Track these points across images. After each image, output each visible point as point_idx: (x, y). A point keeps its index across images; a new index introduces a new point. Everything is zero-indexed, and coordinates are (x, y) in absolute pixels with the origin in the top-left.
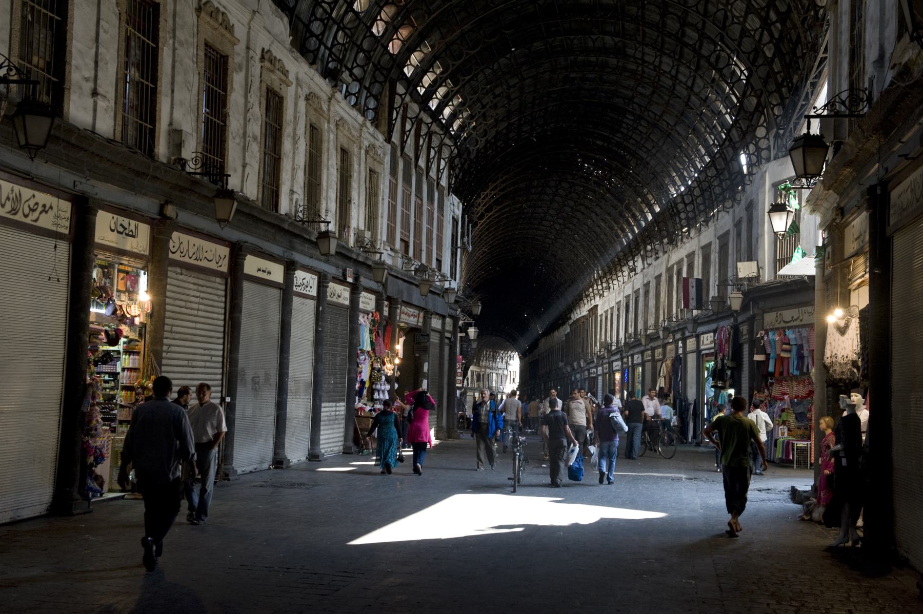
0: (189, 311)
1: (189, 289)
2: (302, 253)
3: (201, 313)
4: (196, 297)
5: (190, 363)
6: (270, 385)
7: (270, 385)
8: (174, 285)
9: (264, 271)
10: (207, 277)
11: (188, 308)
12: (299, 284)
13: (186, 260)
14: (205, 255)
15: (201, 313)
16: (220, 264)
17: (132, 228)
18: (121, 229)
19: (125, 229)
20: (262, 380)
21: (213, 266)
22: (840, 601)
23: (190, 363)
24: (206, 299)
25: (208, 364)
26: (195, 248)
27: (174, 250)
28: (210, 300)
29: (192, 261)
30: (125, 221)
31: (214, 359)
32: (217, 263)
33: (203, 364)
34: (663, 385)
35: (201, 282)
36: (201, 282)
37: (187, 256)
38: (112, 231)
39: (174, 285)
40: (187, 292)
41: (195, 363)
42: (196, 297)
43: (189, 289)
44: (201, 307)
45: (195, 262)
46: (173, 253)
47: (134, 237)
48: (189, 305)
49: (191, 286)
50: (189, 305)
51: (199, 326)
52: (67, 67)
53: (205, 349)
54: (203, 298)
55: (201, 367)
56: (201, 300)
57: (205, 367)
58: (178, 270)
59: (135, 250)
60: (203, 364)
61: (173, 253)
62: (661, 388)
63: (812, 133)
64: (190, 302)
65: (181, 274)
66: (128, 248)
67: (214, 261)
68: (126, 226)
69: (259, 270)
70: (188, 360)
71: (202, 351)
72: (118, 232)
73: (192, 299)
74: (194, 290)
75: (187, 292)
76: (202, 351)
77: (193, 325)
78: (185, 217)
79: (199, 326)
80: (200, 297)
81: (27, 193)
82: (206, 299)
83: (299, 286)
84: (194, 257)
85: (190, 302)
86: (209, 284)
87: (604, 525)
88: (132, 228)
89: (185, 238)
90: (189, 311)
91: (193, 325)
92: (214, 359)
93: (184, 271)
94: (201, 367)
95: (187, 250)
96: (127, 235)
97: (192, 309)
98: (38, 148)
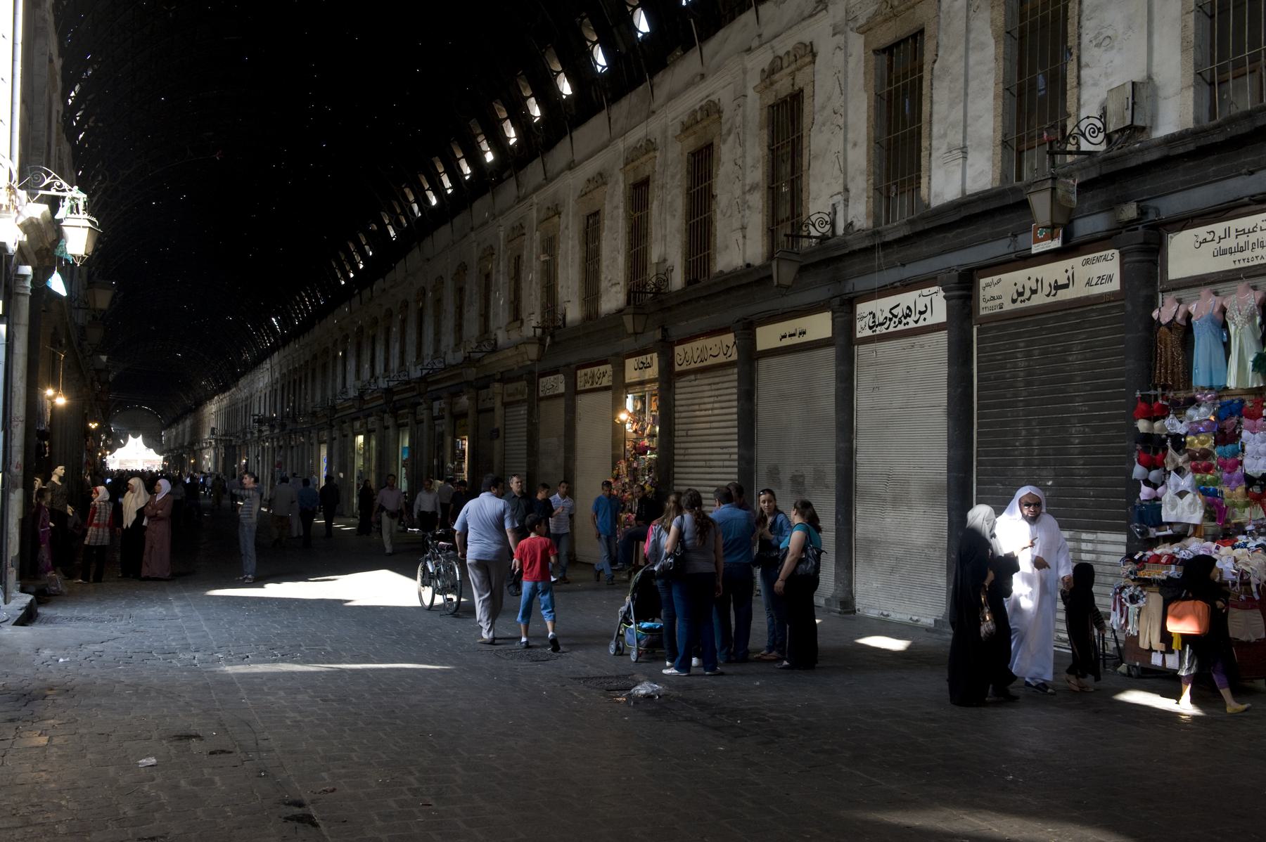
0: (703, 413)
2: (862, 273)
3: (716, 412)
5: (708, 463)
9: (794, 335)
10: (724, 372)
11: (701, 410)
13: (693, 366)
15: (716, 412)
17: (649, 360)
18: (641, 366)
21: (722, 359)
23: (708, 463)
24: (721, 395)
25: (727, 463)
26: (699, 351)
28: (727, 395)
30: (642, 358)
32: (725, 355)
33: (721, 463)
34: (213, 425)
37: (693, 363)
44: (716, 405)
46: (680, 365)
47: (650, 367)
48: (703, 407)
50: (703, 407)
52: (1000, 110)
54: (717, 396)
55: (720, 467)
56: (716, 399)
57: (723, 467)
58: (693, 377)
60: (721, 463)
61: (680, 365)
62: (213, 429)
64: (705, 403)
67: (721, 354)
68: (644, 361)
69: (784, 337)
70: (705, 461)
72: (640, 369)
73: (706, 400)
74: (709, 391)
77: (708, 425)
81: (596, 369)
82: (721, 395)
85: (705, 403)
86: (725, 379)
87: (259, 582)
89: (687, 347)
90: (703, 413)
91: (708, 425)
93: (699, 376)
94: (720, 467)
95: (692, 357)
96: (646, 368)
97: (706, 410)
98: (788, 287)
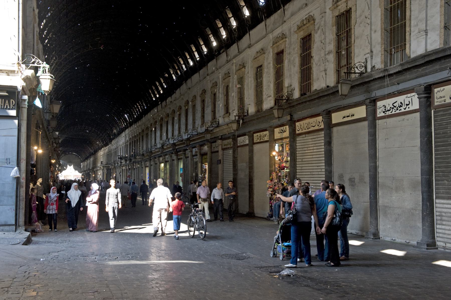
1: (309, 142)
3: (315, 151)
4: (312, 144)
6: (365, 183)
7: (365, 183)
8: (302, 143)
11: (308, 150)
12: (389, 109)
13: (304, 131)
14: (311, 125)
15: (315, 151)
16: (320, 125)
17: (285, 129)
18: (281, 131)
19: (282, 130)
20: (357, 180)
22: (348, 294)
27: (298, 130)
29: (306, 130)
30: (282, 128)
31: (300, 168)
32: (318, 126)
33: (317, 173)
35: (315, 137)
36: (315, 137)
38: (279, 133)
39: (302, 143)
40: (308, 143)
41: (313, 173)
42: (312, 144)
43: (309, 142)
44: (315, 148)
45: (308, 130)
48: (309, 149)
49: (310, 140)
50: (309, 149)
51: (314, 156)
53: (318, 166)
55: (317, 175)
56: (314, 145)
58: (304, 136)
59: (286, 136)
60: (317, 173)
63: (203, 43)
65: (305, 137)
66: (284, 136)
67: (317, 126)
69: (344, 117)
70: (310, 172)
71: (317, 168)
75: (308, 143)
76: (317, 168)
78: (379, 93)
79: (314, 156)
80: (314, 144)
81: (262, 133)
83: (389, 110)
84: (307, 128)
88: (285, 129)
91: (311, 157)
92: (300, 168)
93: (307, 135)
94: (317, 175)
95: (304, 127)
96: (283, 132)
98: (346, 96)
